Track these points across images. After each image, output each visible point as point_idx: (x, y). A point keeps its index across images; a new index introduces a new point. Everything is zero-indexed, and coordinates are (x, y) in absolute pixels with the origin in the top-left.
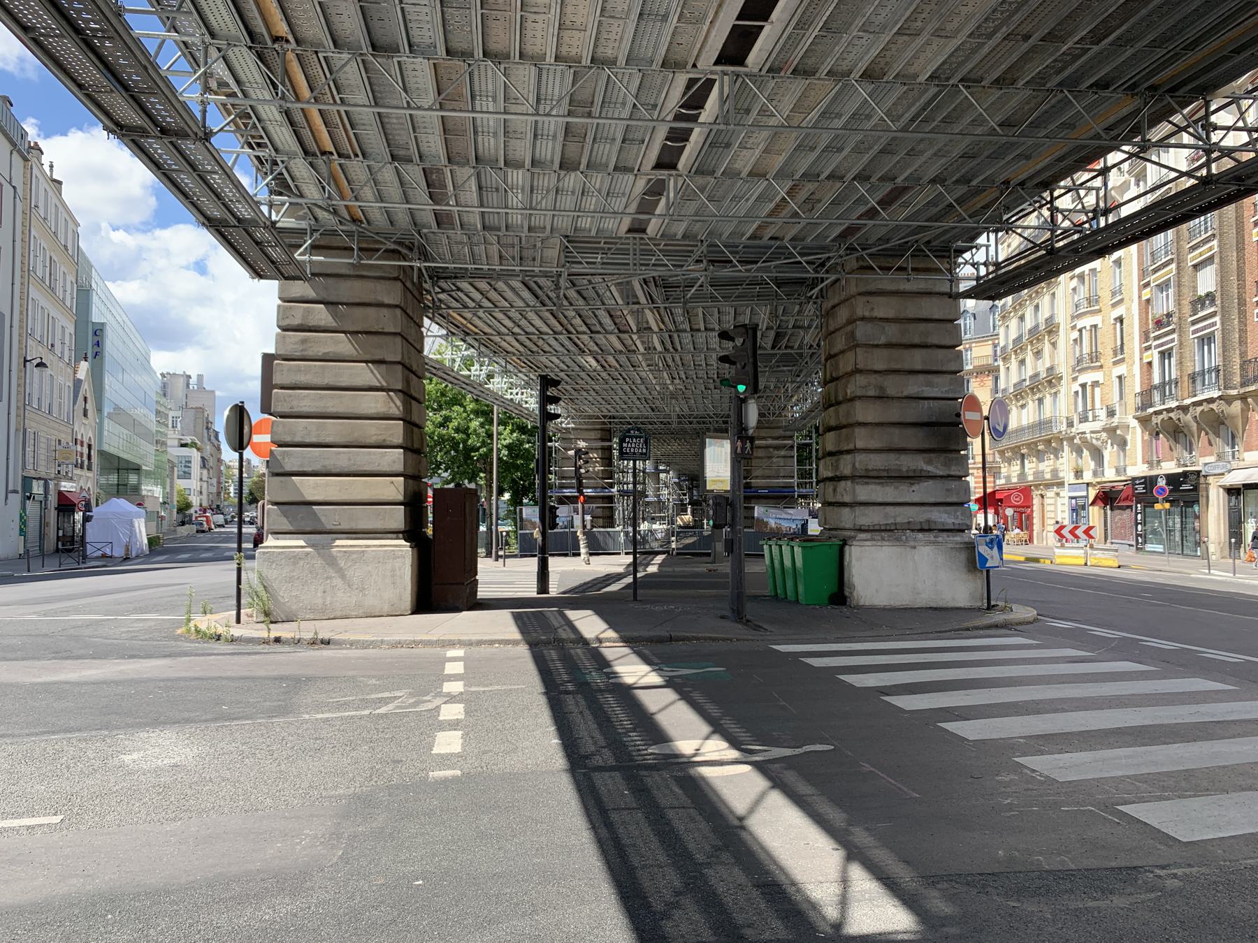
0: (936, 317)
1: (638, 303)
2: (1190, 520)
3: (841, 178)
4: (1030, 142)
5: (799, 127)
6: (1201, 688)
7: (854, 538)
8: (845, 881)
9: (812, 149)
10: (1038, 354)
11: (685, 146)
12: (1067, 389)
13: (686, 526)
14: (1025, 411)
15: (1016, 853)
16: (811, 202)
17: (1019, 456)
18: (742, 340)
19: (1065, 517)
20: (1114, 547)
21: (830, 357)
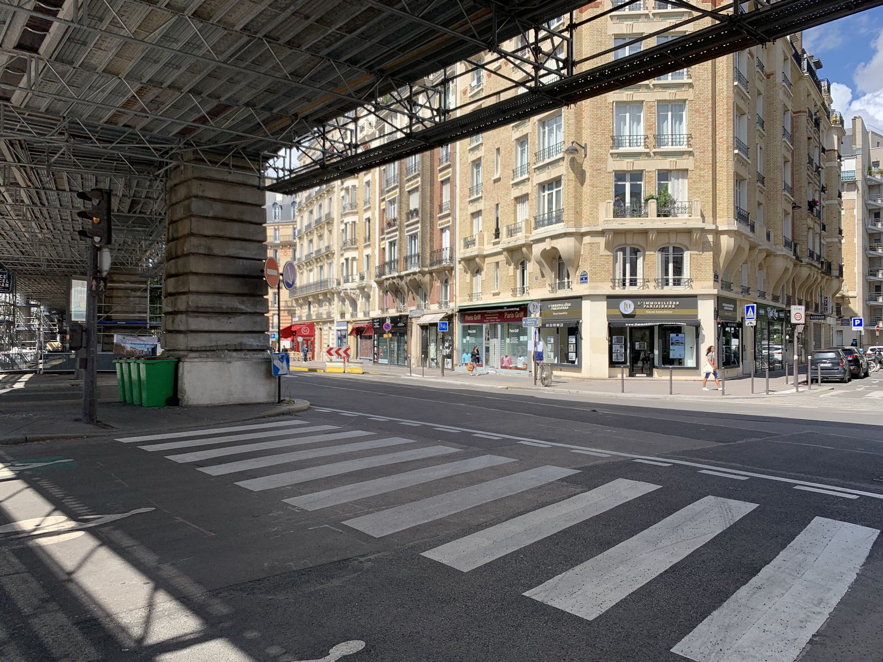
0: (249, 201)
1: (5, 161)
2: (402, 344)
3: (179, 89)
4: (310, 89)
5: (142, 41)
6: (397, 443)
7: (186, 356)
8: (151, 606)
9: (156, 62)
10: (321, 237)
11: (45, 35)
12: (338, 261)
13: (55, 351)
14: (311, 274)
15: (276, 563)
16: (155, 103)
17: (307, 303)
18: (98, 201)
19: (333, 343)
20: (361, 361)
21: (172, 222)
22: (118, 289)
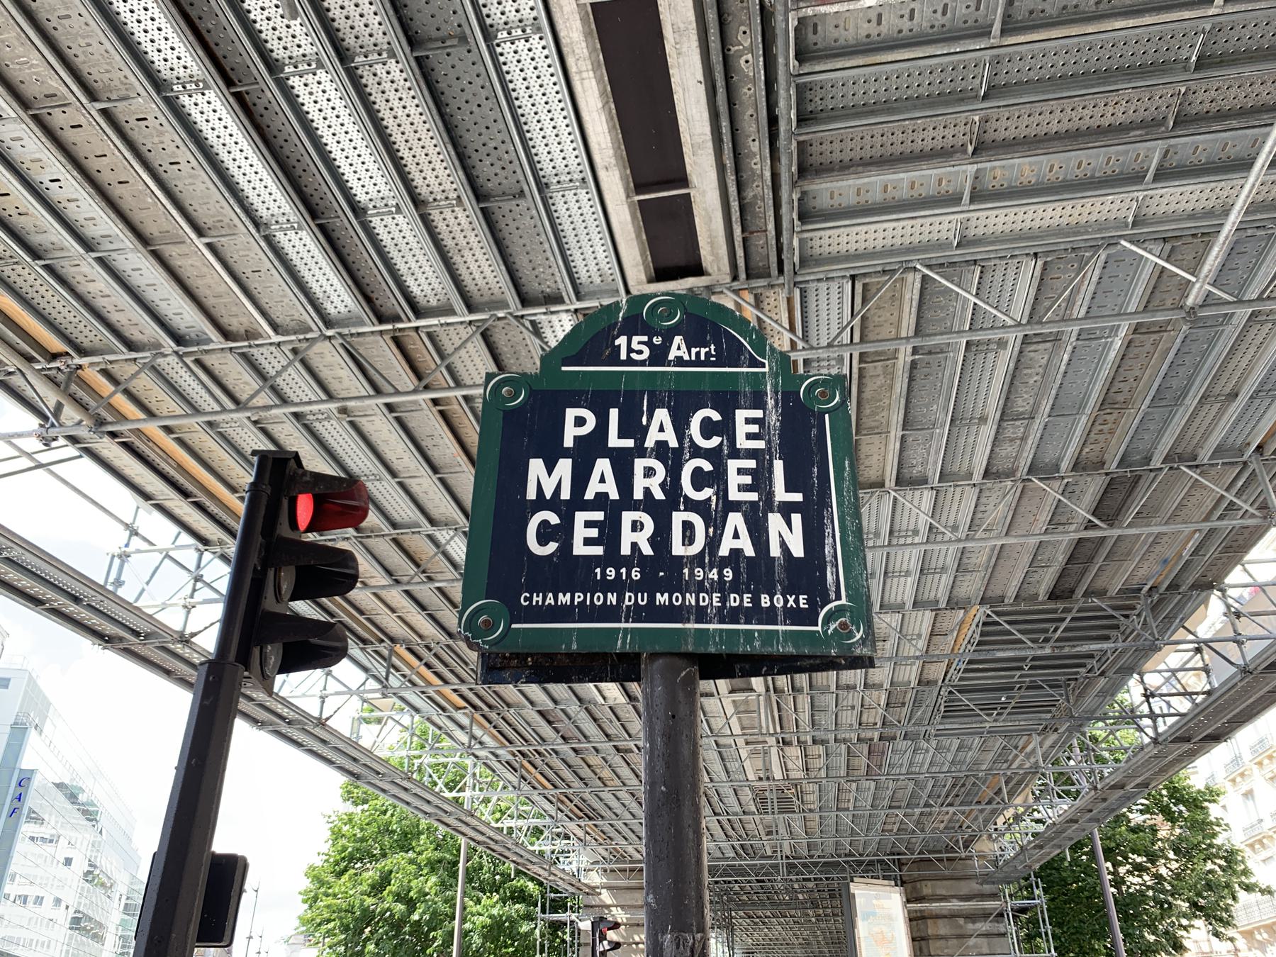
22: (937, 917)
